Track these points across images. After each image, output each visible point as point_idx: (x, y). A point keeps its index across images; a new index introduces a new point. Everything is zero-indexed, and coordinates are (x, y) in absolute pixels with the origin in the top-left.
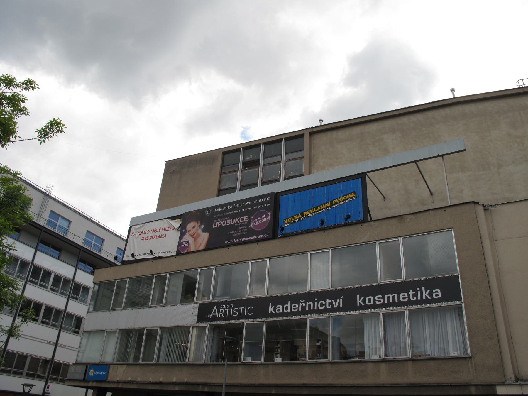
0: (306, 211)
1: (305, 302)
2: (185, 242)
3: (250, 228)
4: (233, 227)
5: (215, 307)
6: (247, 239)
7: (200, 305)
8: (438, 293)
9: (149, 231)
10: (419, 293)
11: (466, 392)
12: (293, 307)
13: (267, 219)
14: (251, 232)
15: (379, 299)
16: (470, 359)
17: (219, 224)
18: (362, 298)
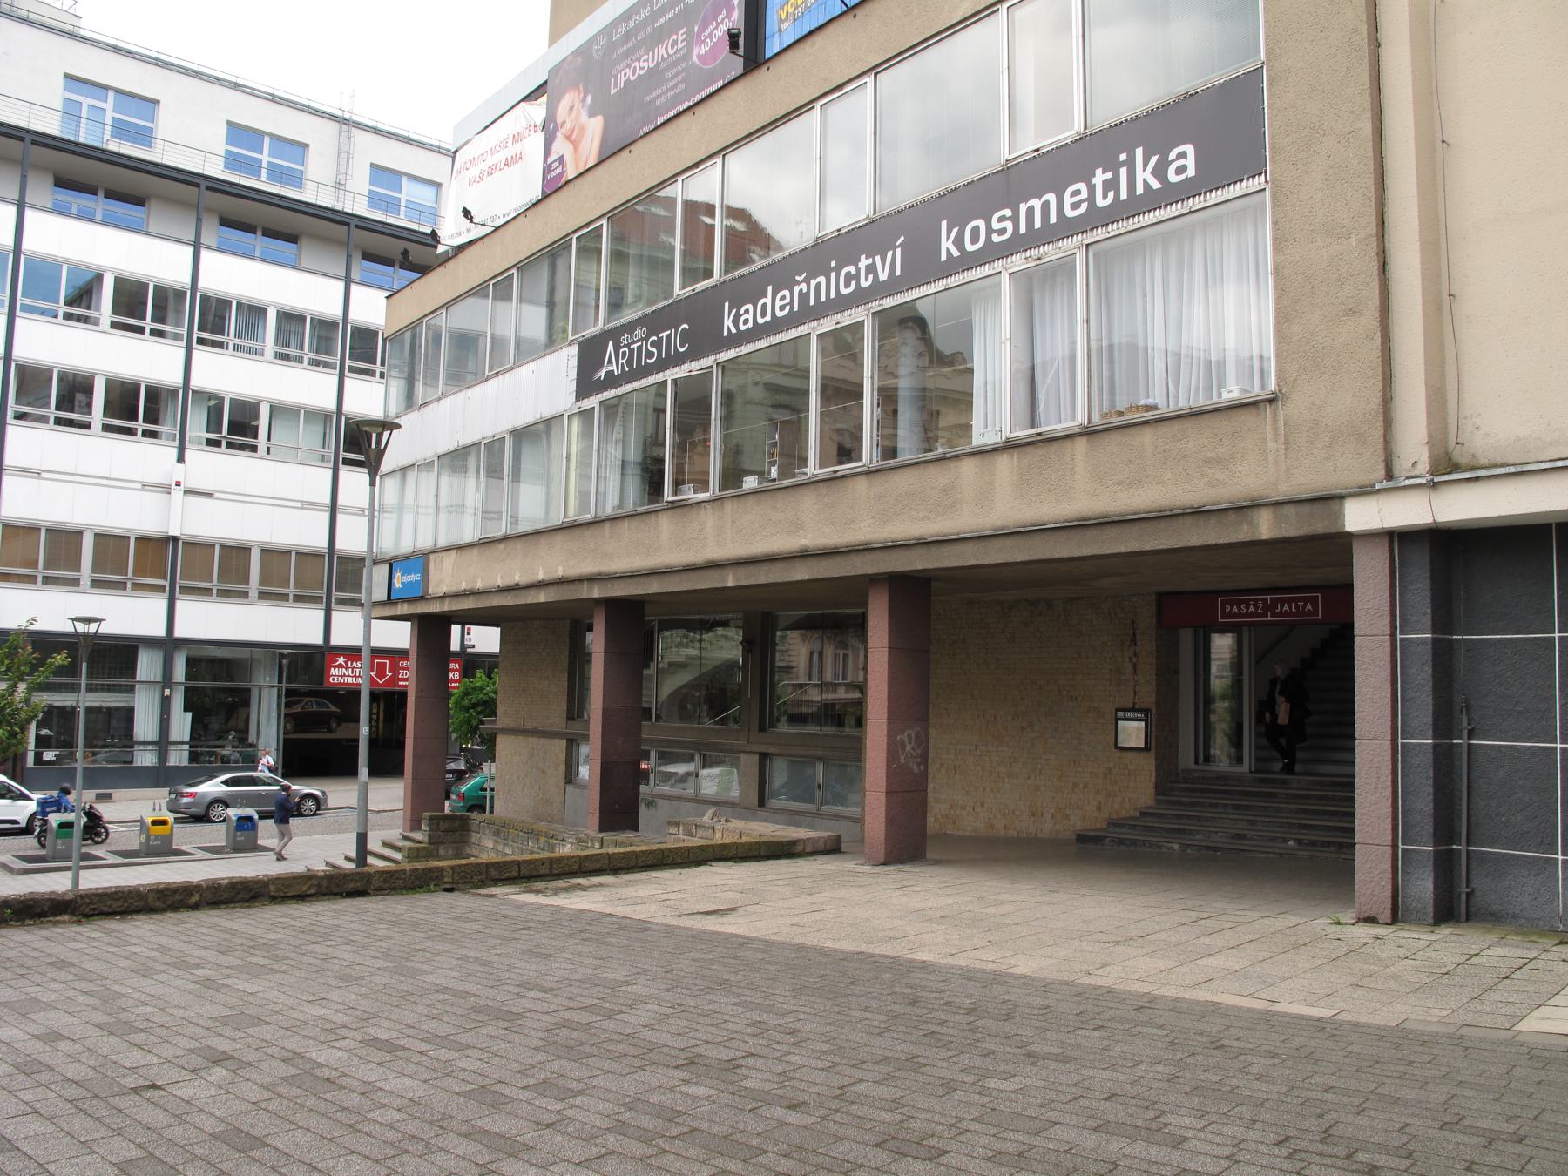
1: (807, 281)
3: (693, 63)
7: (581, 345)
8: (1185, 160)
10: (1123, 171)
11: (1241, 534)
13: (730, 21)
15: (1002, 225)
16: (1271, 405)
17: (623, 79)
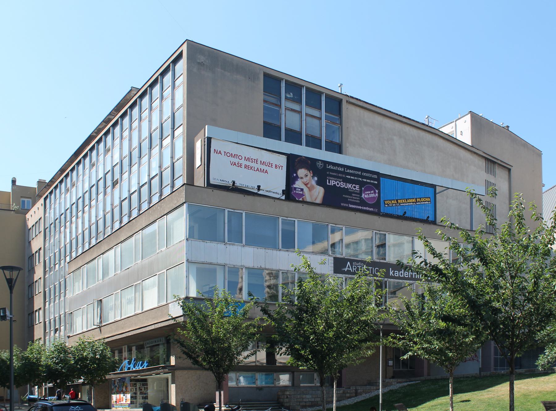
0: (400, 200)
2: (299, 188)
3: (362, 198)
4: (346, 191)
5: (349, 263)
6: (360, 207)
9: (241, 158)
12: (405, 274)
14: (363, 202)
18: (393, 271)
